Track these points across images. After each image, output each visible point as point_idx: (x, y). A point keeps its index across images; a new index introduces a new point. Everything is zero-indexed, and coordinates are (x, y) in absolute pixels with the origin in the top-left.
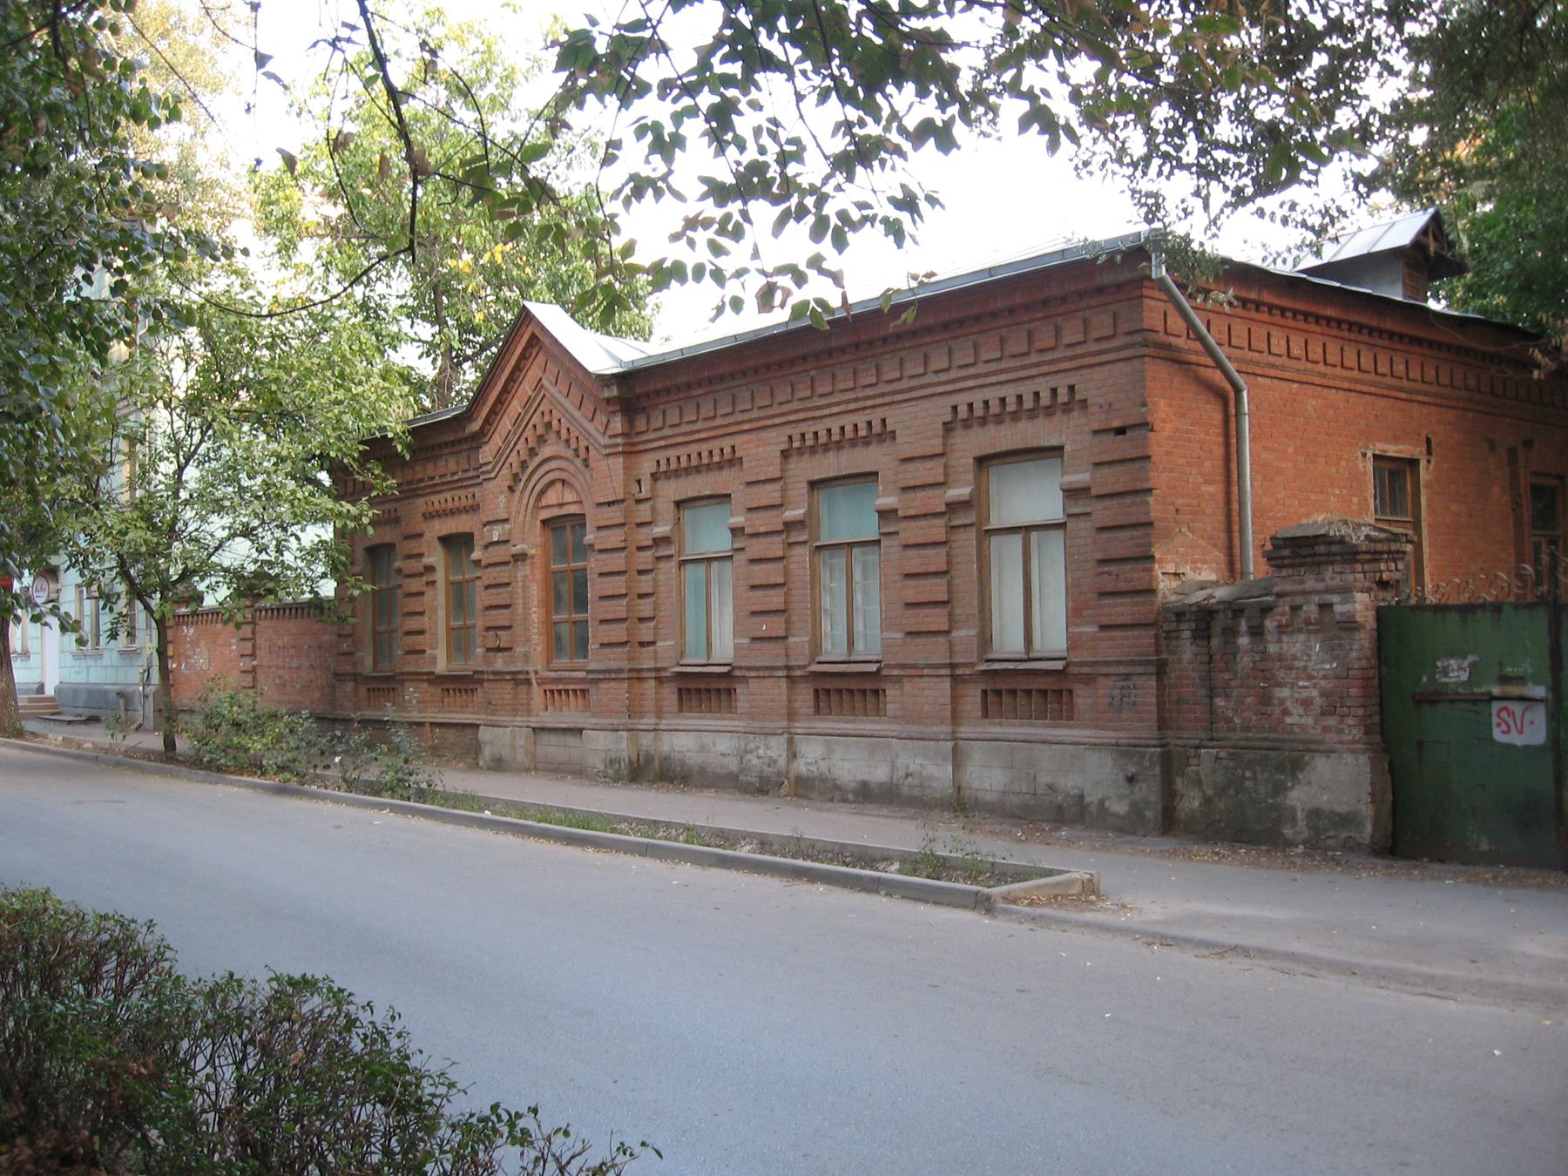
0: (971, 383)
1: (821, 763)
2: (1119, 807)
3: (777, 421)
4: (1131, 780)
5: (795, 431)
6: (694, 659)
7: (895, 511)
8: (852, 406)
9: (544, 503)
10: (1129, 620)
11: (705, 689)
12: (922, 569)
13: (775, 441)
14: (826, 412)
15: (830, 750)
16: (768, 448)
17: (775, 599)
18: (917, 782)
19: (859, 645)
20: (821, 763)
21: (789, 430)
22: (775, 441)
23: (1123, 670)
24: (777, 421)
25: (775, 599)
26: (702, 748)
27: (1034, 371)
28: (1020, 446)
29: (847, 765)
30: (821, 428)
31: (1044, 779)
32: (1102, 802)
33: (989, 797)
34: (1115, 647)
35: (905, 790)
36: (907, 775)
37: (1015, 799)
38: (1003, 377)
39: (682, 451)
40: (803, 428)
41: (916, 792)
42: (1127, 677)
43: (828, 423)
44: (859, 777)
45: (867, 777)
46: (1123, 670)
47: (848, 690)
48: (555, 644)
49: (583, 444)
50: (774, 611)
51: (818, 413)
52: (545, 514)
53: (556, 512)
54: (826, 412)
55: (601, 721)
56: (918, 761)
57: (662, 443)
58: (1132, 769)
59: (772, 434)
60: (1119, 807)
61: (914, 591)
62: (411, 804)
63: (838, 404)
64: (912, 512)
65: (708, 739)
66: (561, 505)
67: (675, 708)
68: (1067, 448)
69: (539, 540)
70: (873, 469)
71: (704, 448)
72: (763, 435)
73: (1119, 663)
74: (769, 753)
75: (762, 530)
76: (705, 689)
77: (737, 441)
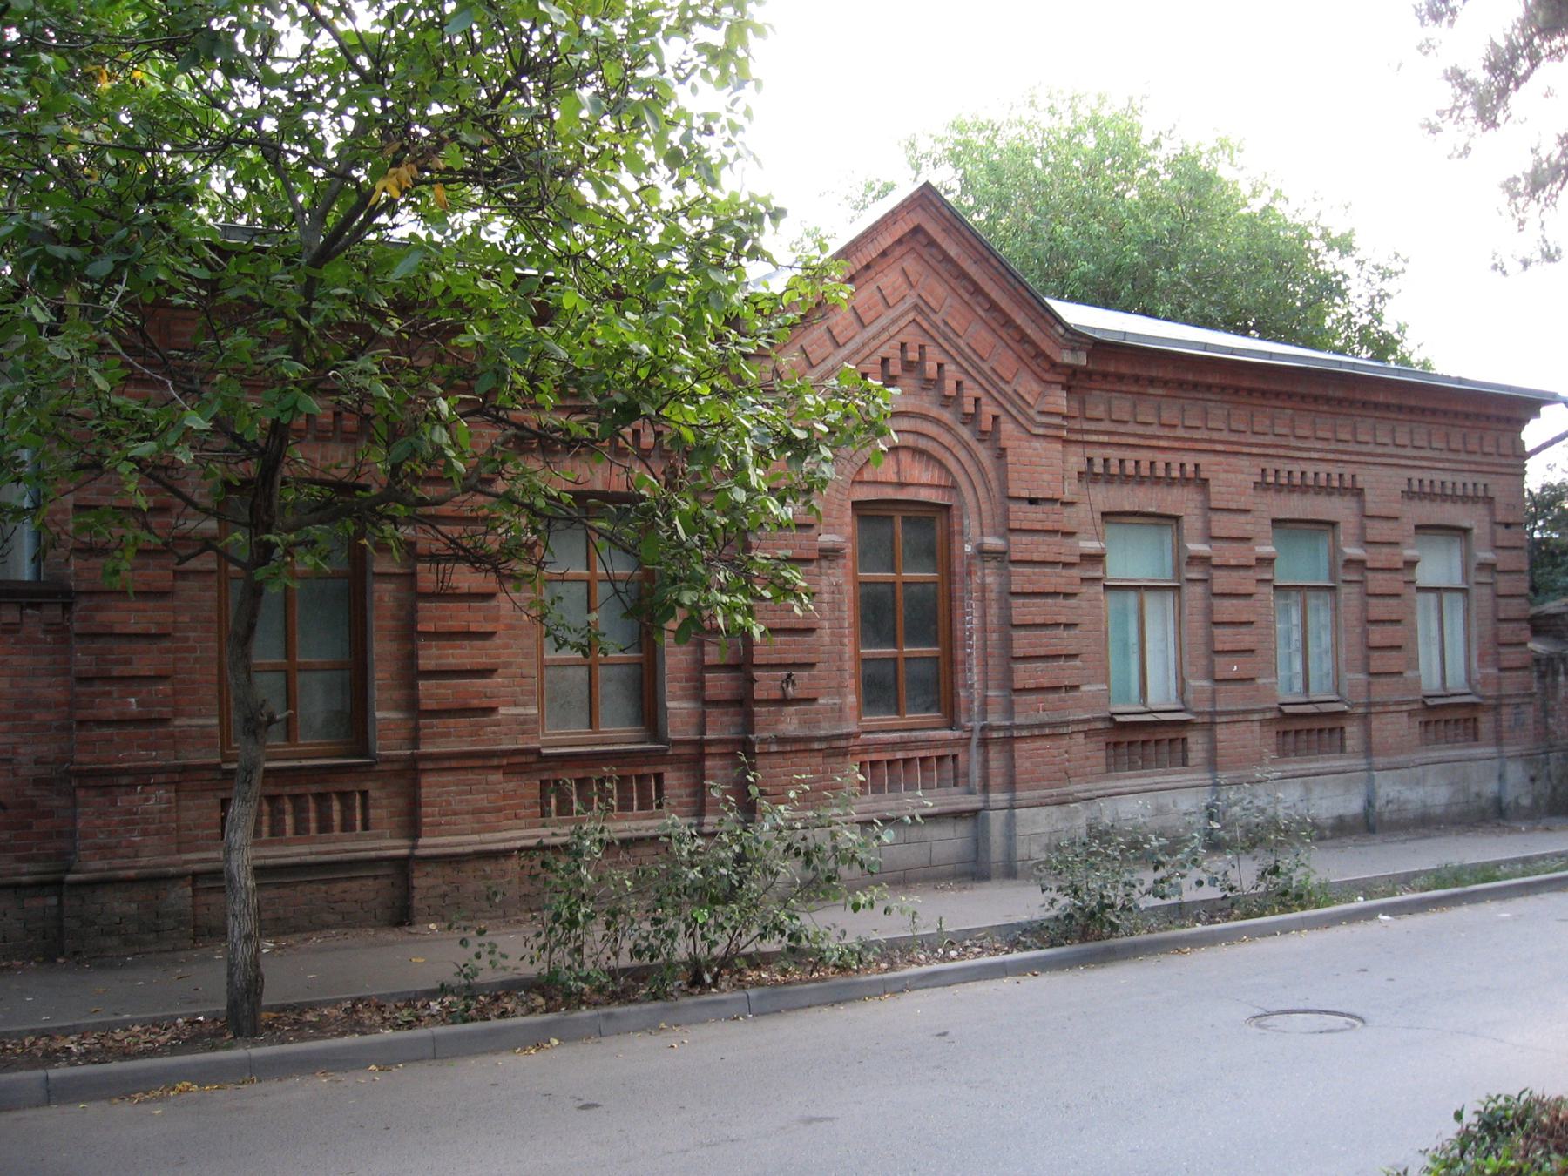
0: (1424, 463)
1: (1300, 805)
2: (1526, 801)
3: (1255, 450)
4: (1533, 780)
5: (1271, 465)
6: (1126, 706)
7: (1209, 558)
8: (1331, 456)
9: (867, 476)
10: (1518, 664)
11: (1139, 741)
12: (1386, 617)
13: (1396, 480)
14: (1305, 455)
15: (1308, 790)
16: (1241, 477)
17: (1377, 636)
18: (1396, 807)
19: (1313, 686)
20: (1300, 805)
21: (1263, 463)
22: (1396, 480)
23: (1517, 700)
24: (1255, 450)
25: (1377, 636)
26: (1160, 810)
27: (1466, 467)
28: (1446, 522)
29: (1325, 803)
30: (1296, 468)
31: (1474, 789)
32: (1517, 799)
33: (1439, 811)
34: (1512, 684)
35: (1386, 816)
36: (1388, 802)
37: (1455, 809)
38: (1447, 465)
39: (1130, 456)
40: (1277, 464)
41: (1395, 817)
42: (1518, 705)
43: (1304, 466)
44: (1336, 813)
45: (1341, 812)
46: (1517, 700)
47: (1306, 730)
48: (879, 688)
49: (989, 409)
50: (1221, 647)
51: (1298, 454)
52: (863, 494)
53: (890, 493)
54: (1305, 455)
55: (1037, 793)
56: (1398, 788)
57: (1105, 439)
58: (1532, 772)
59: (1244, 462)
60: (1526, 801)
61: (1245, 638)
62: (1157, 935)
63: (1351, 453)
64: (1378, 565)
65: (1166, 799)
66: (902, 485)
67: (1102, 768)
68: (1475, 531)
69: (848, 530)
70: (1332, 518)
71: (1161, 459)
72: (1233, 460)
73: (1517, 695)
74: (1256, 802)
75: (1233, 562)
76: (1139, 741)
77: (1203, 460)
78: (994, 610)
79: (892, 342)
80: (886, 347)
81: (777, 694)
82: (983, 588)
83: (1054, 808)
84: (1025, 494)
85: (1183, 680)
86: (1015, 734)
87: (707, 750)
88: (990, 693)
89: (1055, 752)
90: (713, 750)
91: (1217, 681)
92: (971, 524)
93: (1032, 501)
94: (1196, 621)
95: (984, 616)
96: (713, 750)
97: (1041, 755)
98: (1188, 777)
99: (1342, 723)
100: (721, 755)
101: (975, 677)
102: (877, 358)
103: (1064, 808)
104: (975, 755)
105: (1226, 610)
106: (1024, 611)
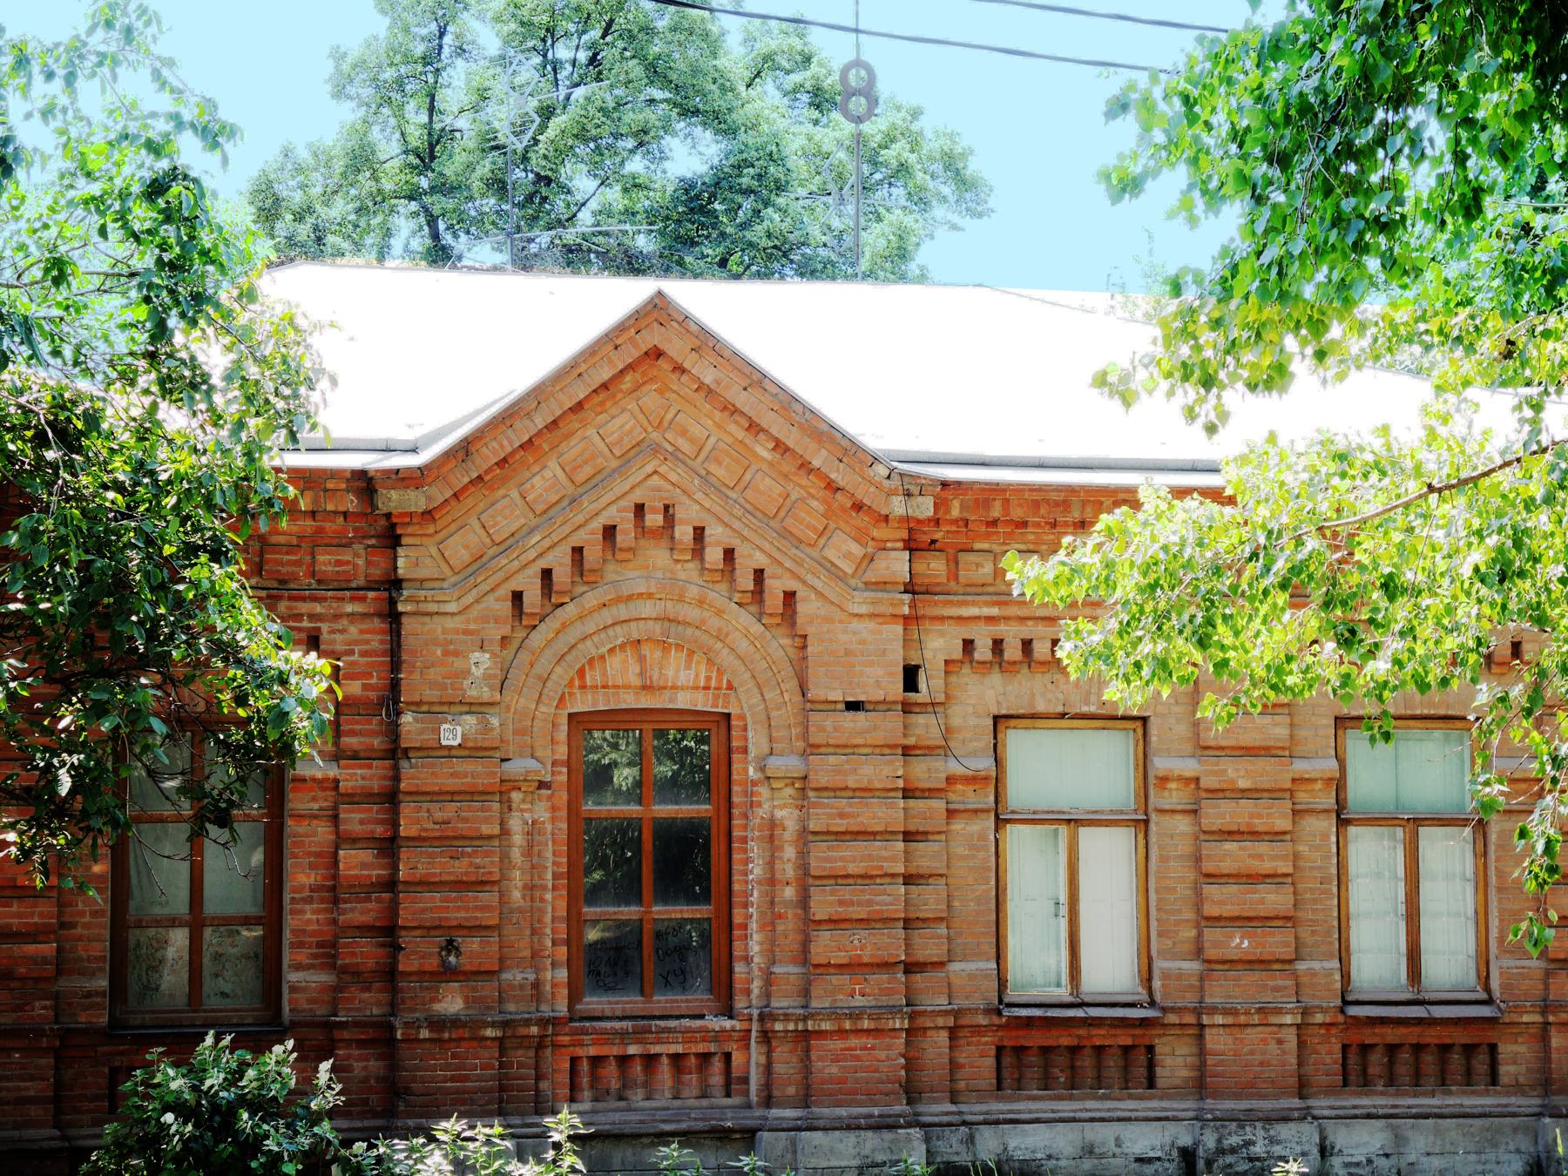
55: (843, 1112)
65: (1103, 1134)
78: (789, 852)
79: (623, 503)
80: (613, 510)
81: (433, 963)
82: (773, 825)
83: (870, 1134)
84: (836, 695)
85: (1150, 959)
86: (810, 1025)
87: (337, 1034)
88: (777, 969)
89: (882, 1055)
90: (346, 1035)
91: (1208, 962)
92: (756, 741)
93: (854, 706)
94: (1180, 875)
95: (771, 864)
96: (346, 1035)
97: (857, 1058)
98: (1154, 1104)
99: (1491, 1035)
100: (361, 1044)
101: (755, 945)
102: (629, 503)
103: (888, 1135)
104: (756, 1054)
105: (1231, 856)
106: (824, 857)
